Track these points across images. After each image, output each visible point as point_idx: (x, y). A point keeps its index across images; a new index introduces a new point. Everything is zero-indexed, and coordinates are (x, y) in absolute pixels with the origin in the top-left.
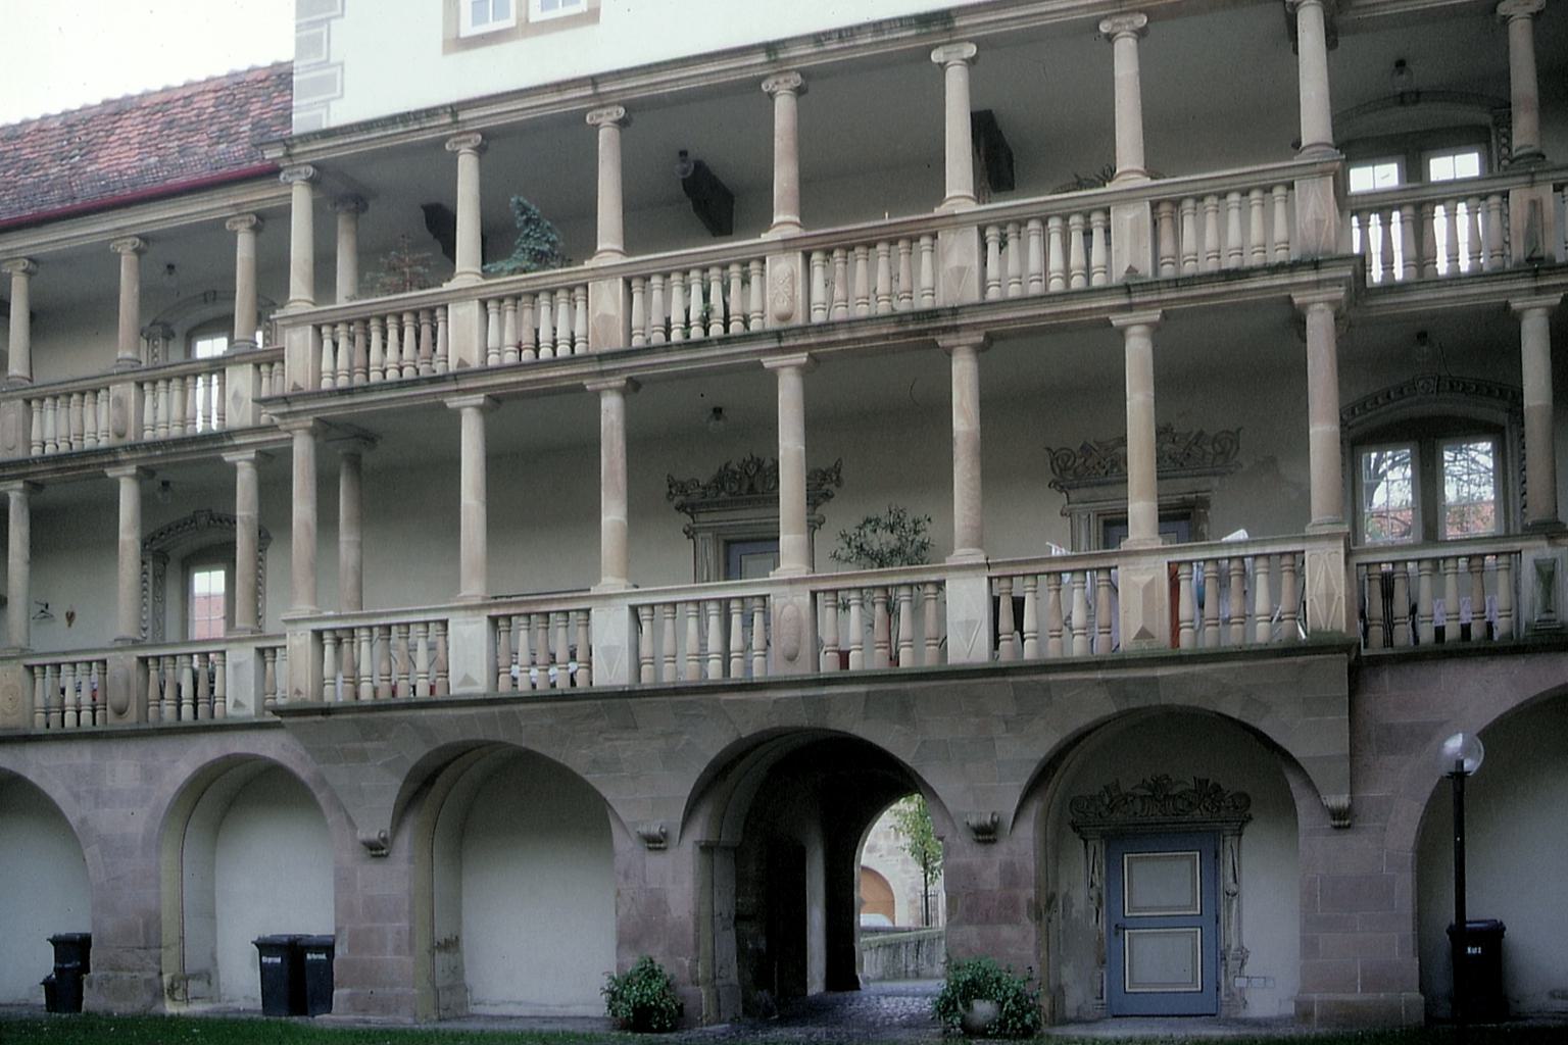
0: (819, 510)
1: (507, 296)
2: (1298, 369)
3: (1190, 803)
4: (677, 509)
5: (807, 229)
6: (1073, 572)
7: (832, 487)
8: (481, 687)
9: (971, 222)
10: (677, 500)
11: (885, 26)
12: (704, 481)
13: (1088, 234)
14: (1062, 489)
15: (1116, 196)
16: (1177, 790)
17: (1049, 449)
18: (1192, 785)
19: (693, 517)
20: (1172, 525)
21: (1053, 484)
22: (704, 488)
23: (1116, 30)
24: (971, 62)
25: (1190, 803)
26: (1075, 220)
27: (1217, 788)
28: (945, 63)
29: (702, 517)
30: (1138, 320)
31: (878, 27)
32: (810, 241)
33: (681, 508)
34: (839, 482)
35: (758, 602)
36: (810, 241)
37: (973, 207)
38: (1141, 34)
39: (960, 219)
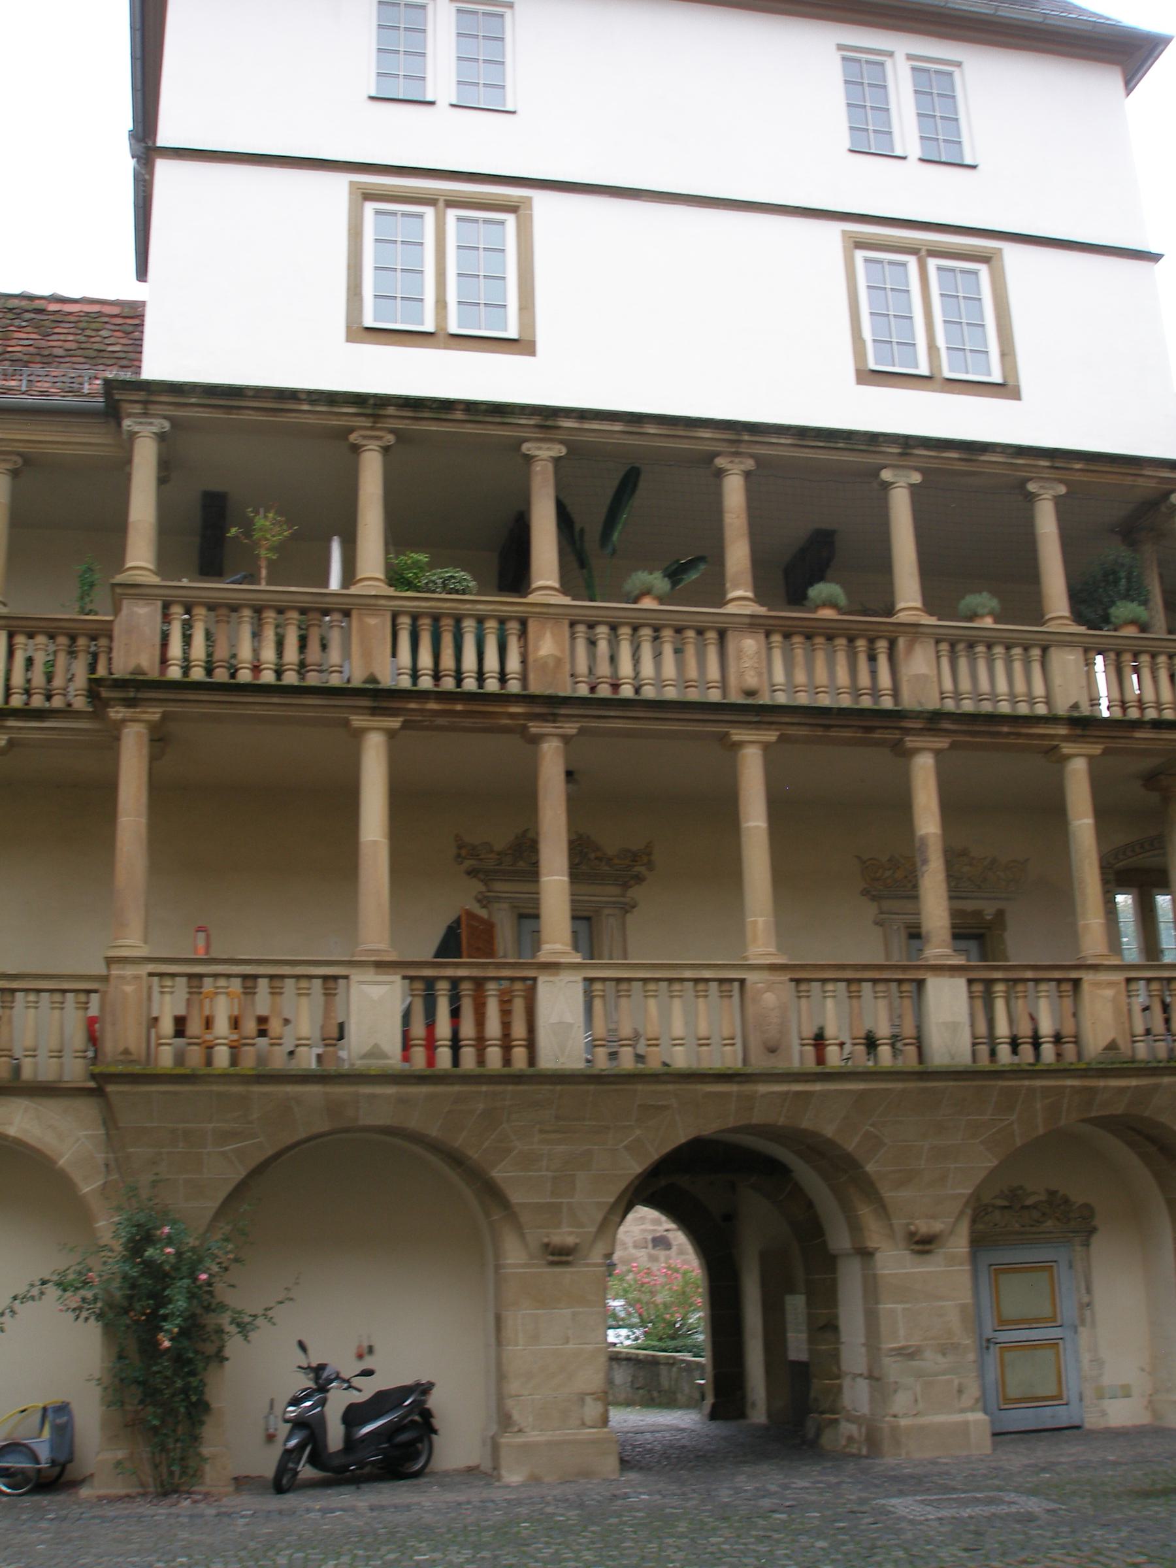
0: (631, 893)
1: (1111, 650)
2: (109, 788)
3: (1044, 1214)
4: (469, 873)
5: (163, 579)
6: (875, 981)
7: (642, 869)
8: (964, 1058)
9: (760, 625)
10: (468, 863)
11: (881, 439)
12: (498, 847)
13: (872, 658)
14: (874, 898)
15: (538, 610)
16: (1030, 1201)
17: (858, 857)
18: (1043, 1198)
19: (486, 884)
20: (963, 944)
21: (865, 893)
22: (499, 854)
23: (1042, 492)
24: (557, 461)
25: (1044, 1214)
26: (491, 625)
27: (1066, 1201)
28: (893, 483)
29: (499, 886)
30: (376, 724)
31: (802, 432)
32: (771, 622)
33: (472, 873)
34: (650, 866)
35: (736, 985)
36: (771, 622)
37: (155, 580)
38: (747, 475)
39: (921, 630)
